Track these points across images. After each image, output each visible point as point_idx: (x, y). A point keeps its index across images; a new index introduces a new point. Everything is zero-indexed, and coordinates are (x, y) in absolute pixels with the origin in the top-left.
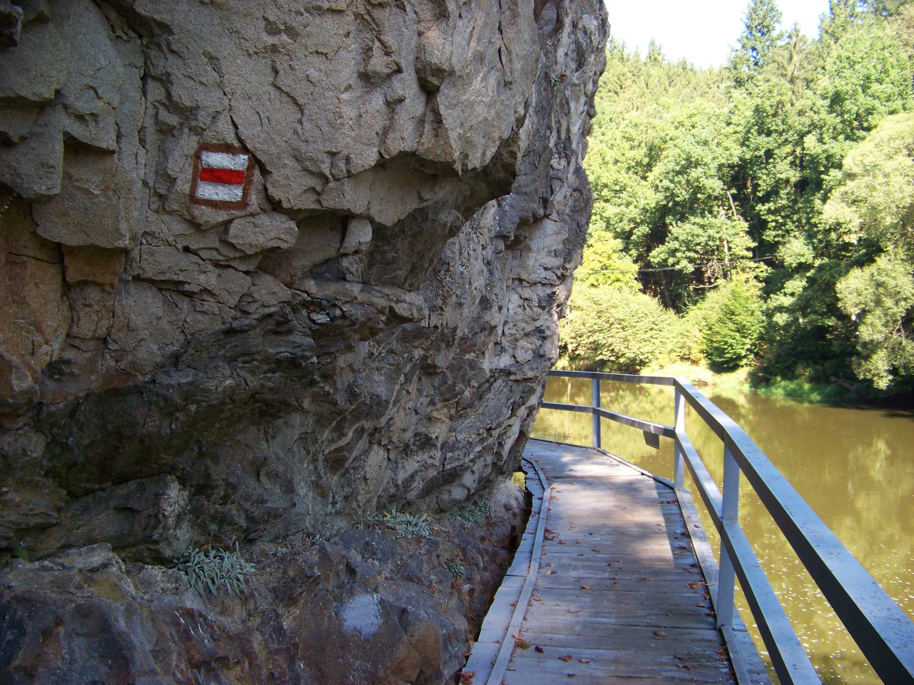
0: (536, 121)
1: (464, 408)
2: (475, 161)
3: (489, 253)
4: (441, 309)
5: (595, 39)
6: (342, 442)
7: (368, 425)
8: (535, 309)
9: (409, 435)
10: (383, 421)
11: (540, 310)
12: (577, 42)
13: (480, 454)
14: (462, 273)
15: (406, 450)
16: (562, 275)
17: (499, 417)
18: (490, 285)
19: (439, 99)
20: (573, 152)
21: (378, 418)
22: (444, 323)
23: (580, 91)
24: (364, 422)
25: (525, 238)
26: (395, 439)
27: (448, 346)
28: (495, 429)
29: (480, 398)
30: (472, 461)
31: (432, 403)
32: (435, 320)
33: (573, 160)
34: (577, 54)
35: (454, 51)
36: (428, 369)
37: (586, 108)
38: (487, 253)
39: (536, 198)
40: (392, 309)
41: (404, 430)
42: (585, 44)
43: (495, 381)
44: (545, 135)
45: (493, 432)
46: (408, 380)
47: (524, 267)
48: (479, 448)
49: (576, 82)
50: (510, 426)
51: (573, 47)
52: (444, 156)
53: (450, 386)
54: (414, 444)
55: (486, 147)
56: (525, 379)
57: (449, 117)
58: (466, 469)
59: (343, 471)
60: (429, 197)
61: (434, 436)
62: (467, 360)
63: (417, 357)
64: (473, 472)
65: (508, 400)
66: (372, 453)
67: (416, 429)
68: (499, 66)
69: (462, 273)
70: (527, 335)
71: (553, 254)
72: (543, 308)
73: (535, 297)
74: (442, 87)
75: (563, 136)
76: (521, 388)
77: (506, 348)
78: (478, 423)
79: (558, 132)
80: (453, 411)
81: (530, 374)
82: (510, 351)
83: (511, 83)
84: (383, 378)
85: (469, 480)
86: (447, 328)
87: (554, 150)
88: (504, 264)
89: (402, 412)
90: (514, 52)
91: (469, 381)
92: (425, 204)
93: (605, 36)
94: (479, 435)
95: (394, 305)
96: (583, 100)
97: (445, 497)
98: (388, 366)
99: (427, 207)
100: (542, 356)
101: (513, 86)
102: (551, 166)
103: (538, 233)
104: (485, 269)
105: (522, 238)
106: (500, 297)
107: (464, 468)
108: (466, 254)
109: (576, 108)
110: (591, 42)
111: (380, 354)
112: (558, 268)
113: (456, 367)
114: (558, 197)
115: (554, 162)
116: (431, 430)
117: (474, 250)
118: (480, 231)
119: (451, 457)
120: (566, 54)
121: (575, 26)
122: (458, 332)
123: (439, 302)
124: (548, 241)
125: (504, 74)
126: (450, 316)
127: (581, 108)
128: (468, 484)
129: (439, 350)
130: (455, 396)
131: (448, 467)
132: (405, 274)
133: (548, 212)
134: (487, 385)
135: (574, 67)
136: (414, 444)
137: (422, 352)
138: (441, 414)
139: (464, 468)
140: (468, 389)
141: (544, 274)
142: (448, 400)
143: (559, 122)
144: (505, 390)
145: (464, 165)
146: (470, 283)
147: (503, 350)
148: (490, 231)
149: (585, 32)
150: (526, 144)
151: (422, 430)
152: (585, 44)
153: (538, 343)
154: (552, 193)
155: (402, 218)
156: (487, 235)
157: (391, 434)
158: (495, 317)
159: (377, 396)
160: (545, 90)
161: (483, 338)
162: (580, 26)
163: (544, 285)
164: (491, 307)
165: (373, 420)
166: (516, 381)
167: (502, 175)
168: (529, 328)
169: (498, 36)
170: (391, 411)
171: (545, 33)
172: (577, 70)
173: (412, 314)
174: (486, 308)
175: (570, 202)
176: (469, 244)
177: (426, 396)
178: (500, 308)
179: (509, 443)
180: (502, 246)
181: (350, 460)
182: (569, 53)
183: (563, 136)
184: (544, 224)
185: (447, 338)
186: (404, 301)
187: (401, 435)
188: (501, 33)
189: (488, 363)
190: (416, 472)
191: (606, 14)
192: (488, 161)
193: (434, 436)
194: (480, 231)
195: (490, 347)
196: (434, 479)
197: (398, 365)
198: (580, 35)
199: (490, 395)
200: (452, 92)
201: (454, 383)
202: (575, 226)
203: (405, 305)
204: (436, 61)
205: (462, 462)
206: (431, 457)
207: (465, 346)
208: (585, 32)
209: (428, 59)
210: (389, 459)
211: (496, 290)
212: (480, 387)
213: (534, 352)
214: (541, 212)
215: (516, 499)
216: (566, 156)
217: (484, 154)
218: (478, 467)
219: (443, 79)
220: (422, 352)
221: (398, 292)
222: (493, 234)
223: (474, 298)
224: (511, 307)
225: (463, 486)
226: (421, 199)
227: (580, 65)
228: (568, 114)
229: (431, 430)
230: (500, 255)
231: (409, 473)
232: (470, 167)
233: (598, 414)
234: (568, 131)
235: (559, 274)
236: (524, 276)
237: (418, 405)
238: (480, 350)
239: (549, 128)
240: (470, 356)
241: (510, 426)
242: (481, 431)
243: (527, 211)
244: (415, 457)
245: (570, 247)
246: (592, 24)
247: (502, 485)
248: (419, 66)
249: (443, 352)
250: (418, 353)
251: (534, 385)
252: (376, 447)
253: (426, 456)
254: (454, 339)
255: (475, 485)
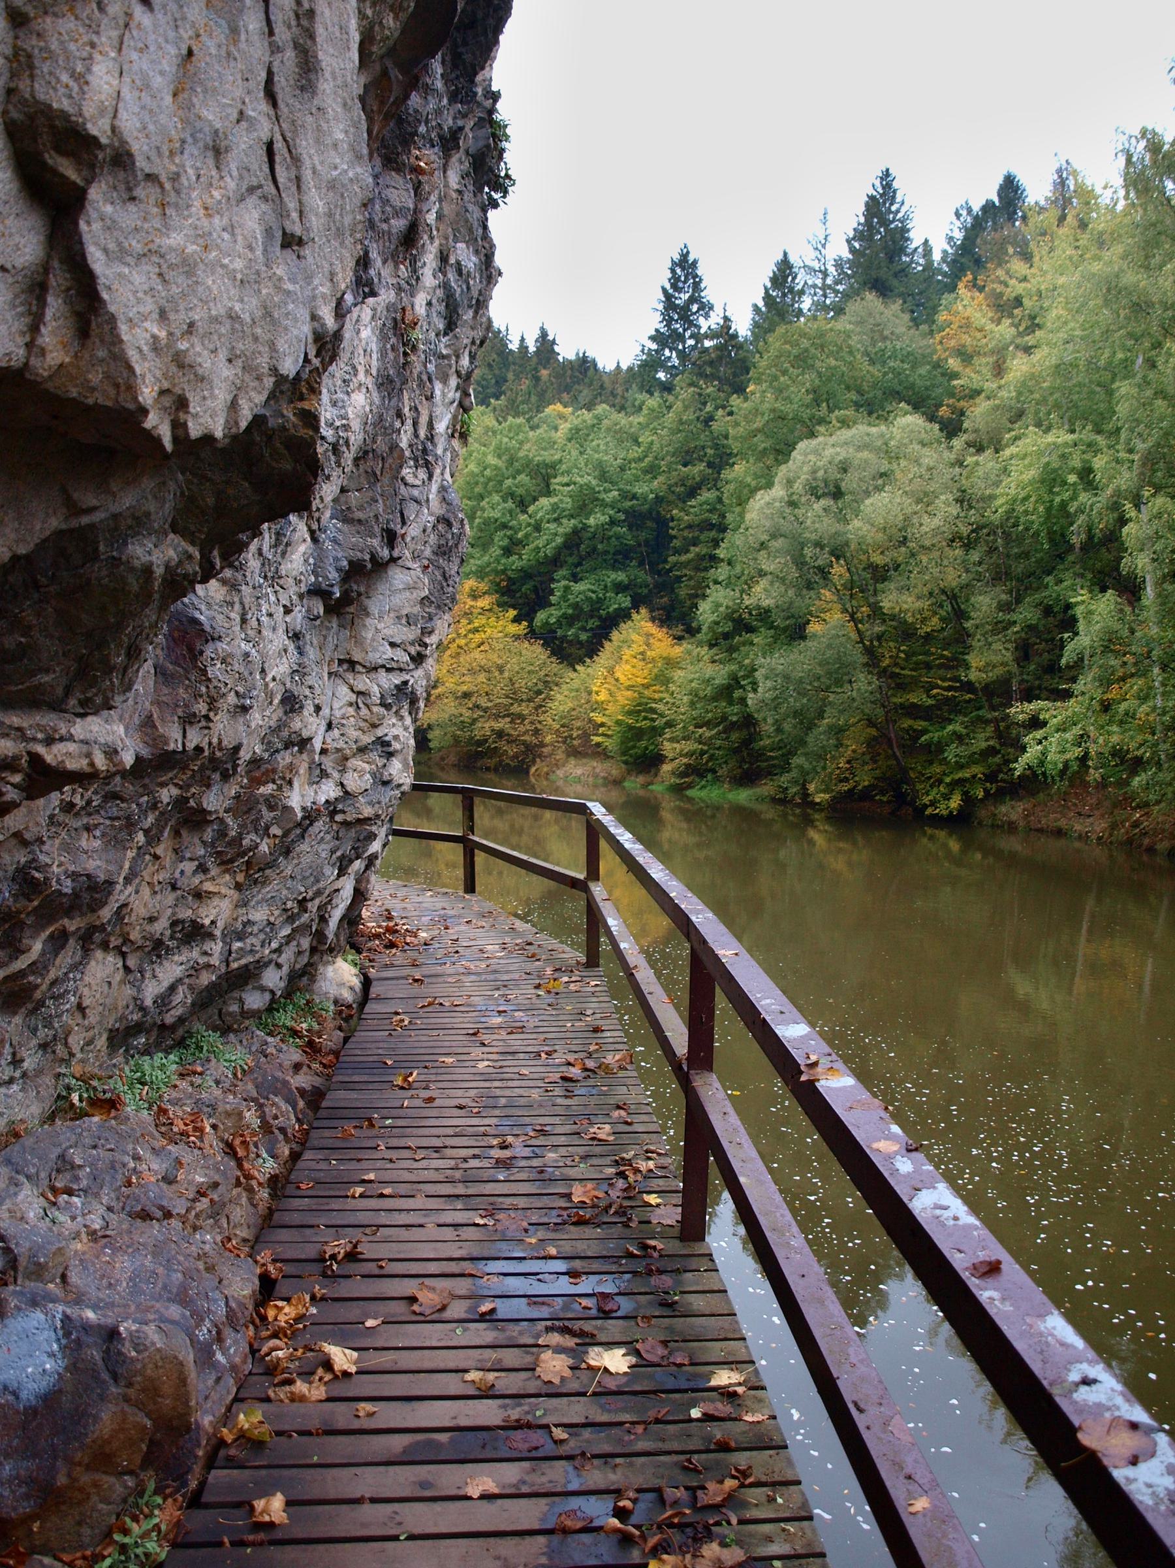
0: (377, 401)
1: (260, 870)
2: (210, 417)
3: (298, 618)
4: (207, 718)
5: (476, 284)
6: (21, 963)
7: (72, 925)
8: (375, 709)
9: (161, 926)
10: (106, 913)
11: (382, 710)
12: (446, 286)
13: (289, 939)
14: (247, 655)
15: (157, 949)
16: (419, 654)
17: (318, 881)
18: (299, 671)
19: (83, 226)
20: (437, 458)
21: (94, 911)
22: (215, 741)
23: (450, 366)
24: (66, 921)
25: (360, 594)
26: (135, 935)
27: (226, 777)
28: (312, 899)
29: (287, 852)
30: (278, 951)
31: (202, 869)
32: (194, 738)
33: (438, 471)
34: (447, 306)
35: (126, 93)
36: (192, 818)
37: (458, 395)
38: (295, 619)
39: (377, 530)
40: (35, 759)
41: (152, 920)
42: (459, 290)
43: (311, 824)
44: (392, 425)
45: (309, 905)
46: (153, 837)
47: (358, 641)
48: (286, 931)
49: (444, 352)
50: (338, 890)
51: (440, 293)
52: (112, 392)
53: (234, 839)
54: (172, 938)
55: (238, 390)
56: (359, 821)
57: (126, 289)
58: (267, 964)
59: (30, 1006)
60: (95, 502)
61: (207, 922)
62: (262, 795)
63: (166, 800)
64: (279, 966)
65: (333, 852)
66: (93, 963)
67: (174, 914)
68: (270, 189)
69: (247, 655)
70: (362, 750)
71: (404, 621)
72: (388, 707)
73: (375, 689)
74: (95, 193)
75: (422, 433)
76: (352, 833)
77: (329, 771)
78: (285, 892)
79: (415, 424)
80: (240, 878)
81: (368, 811)
82: (336, 775)
83: (300, 242)
84: (97, 843)
85: (273, 979)
86: (220, 749)
87: (407, 453)
88: (325, 637)
89: (146, 891)
90: (307, 163)
91: (267, 828)
92: (85, 520)
93: (489, 283)
94: (285, 910)
95: (40, 749)
96: (453, 381)
97: (234, 1008)
98: (108, 822)
99: (92, 526)
100: (385, 783)
101: (307, 251)
102: (403, 479)
103: (382, 587)
104: (291, 647)
105: (354, 595)
106: (318, 691)
107: (261, 965)
108: (254, 623)
109: (444, 395)
110: (468, 288)
111: (89, 802)
112: (412, 644)
113: (244, 806)
114: (413, 531)
115: (406, 472)
116: (203, 912)
117: (270, 615)
118: (281, 582)
119: (241, 949)
120: (429, 304)
121: (443, 258)
122: (242, 753)
123: (201, 707)
124: (397, 600)
125: (283, 214)
126: (224, 728)
127: (451, 395)
128: (271, 985)
129: (208, 786)
130: (244, 853)
131: (235, 965)
132: (64, 681)
133: (396, 554)
134: (298, 831)
135: (441, 326)
136: (172, 938)
137: (175, 792)
138: (221, 884)
139: (261, 965)
140: (266, 840)
141: (389, 652)
142: (232, 861)
143: (415, 409)
144: (328, 837)
145: (178, 427)
146: (263, 671)
147: (324, 774)
148: (298, 582)
149: (460, 272)
150: (361, 437)
151: (185, 914)
152: (459, 290)
153: (380, 762)
154: (404, 523)
155: (22, 550)
156: (293, 590)
157: (127, 929)
158: (311, 725)
159: (88, 876)
160: (393, 348)
161: (288, 759)
162: (452, 261)
163: (389, 670)
164: (302, 707)
165: (83, 915)
166: (345, 824)
167: (287, 466)
168: (367, 739)
169: (264, 106)
170: (122, 894)
171: (394, 231)
172: (446, 334)
173: (92, 764)
174: (292, 710)
175: (433, 539)
176: (259, 605)
177: (191, 859)
178: (318, 709)
179: (337, 914)
180: (320, 609)
181: (44, 987)
182: (434, 301)
183: (422, 433)
184: (390, 573)
185: (220, 763)
186: (71, 738)
187: (148, 928)
188: (275, 105)
189: (298, 798)
190: (180, 981)
191: (492, 246)
192: (243, 425)
193: (207, 922)
194: (281, 582)
195: (302, 771)
196: (212, 986)
197: (128, 818)
198: (452, 276)
199: (304, 847)
200: (129, 216)
201: (240, 834)
202: (440, 578)
203: (71, 747)
204: (66, 105)
205: (257, 956)
206: (205, 953)
207: (257, 774)
208: (460, 272)
209: (41, 97)
210: (127, 969)
211: (310, 680)
212: (285, 835)
213: (373, 775)
214: (385, 553)
215: (351, 988)
216: (427, 464)
217: (233, 406)
218: (286, 957)
219: (92, 167)
220: (175, 792)
221: (49, 719)
222: (304, 589)
223: (270, 696)
224: (336, 705)
225: (263, 989)
226: (75, 510)
227: (451, 326)
228: (430, 398)
229: (203, 912)
230: (318, 622)
231: (166, 984)
232: (195, 431)
233: (470, 849)
234: (430, 426)
235: (413, 652)
236: (357, 657)
237: (177, 875)
238: (284, 778)
239: (399, 415)
240: (267, 789)
241: (338, 890)
242: (289, 904)
243: (361, 551)
244: (176, 958)
245: (432, 610)
246: (470, 261)
247: (330, 968)
248: (15, 115)
249: (215, 789)
250: (166, 795)
251: (374, 828)
252: (99, 954)
253: (195, 954)
254: (235, 766)
255: (282, 985)
